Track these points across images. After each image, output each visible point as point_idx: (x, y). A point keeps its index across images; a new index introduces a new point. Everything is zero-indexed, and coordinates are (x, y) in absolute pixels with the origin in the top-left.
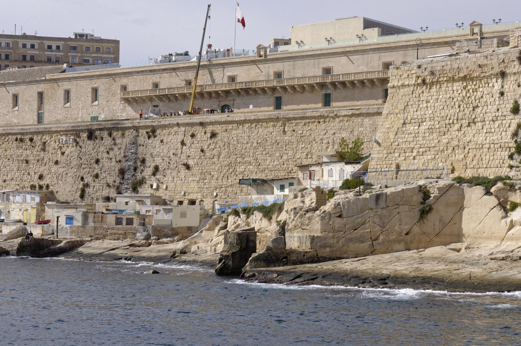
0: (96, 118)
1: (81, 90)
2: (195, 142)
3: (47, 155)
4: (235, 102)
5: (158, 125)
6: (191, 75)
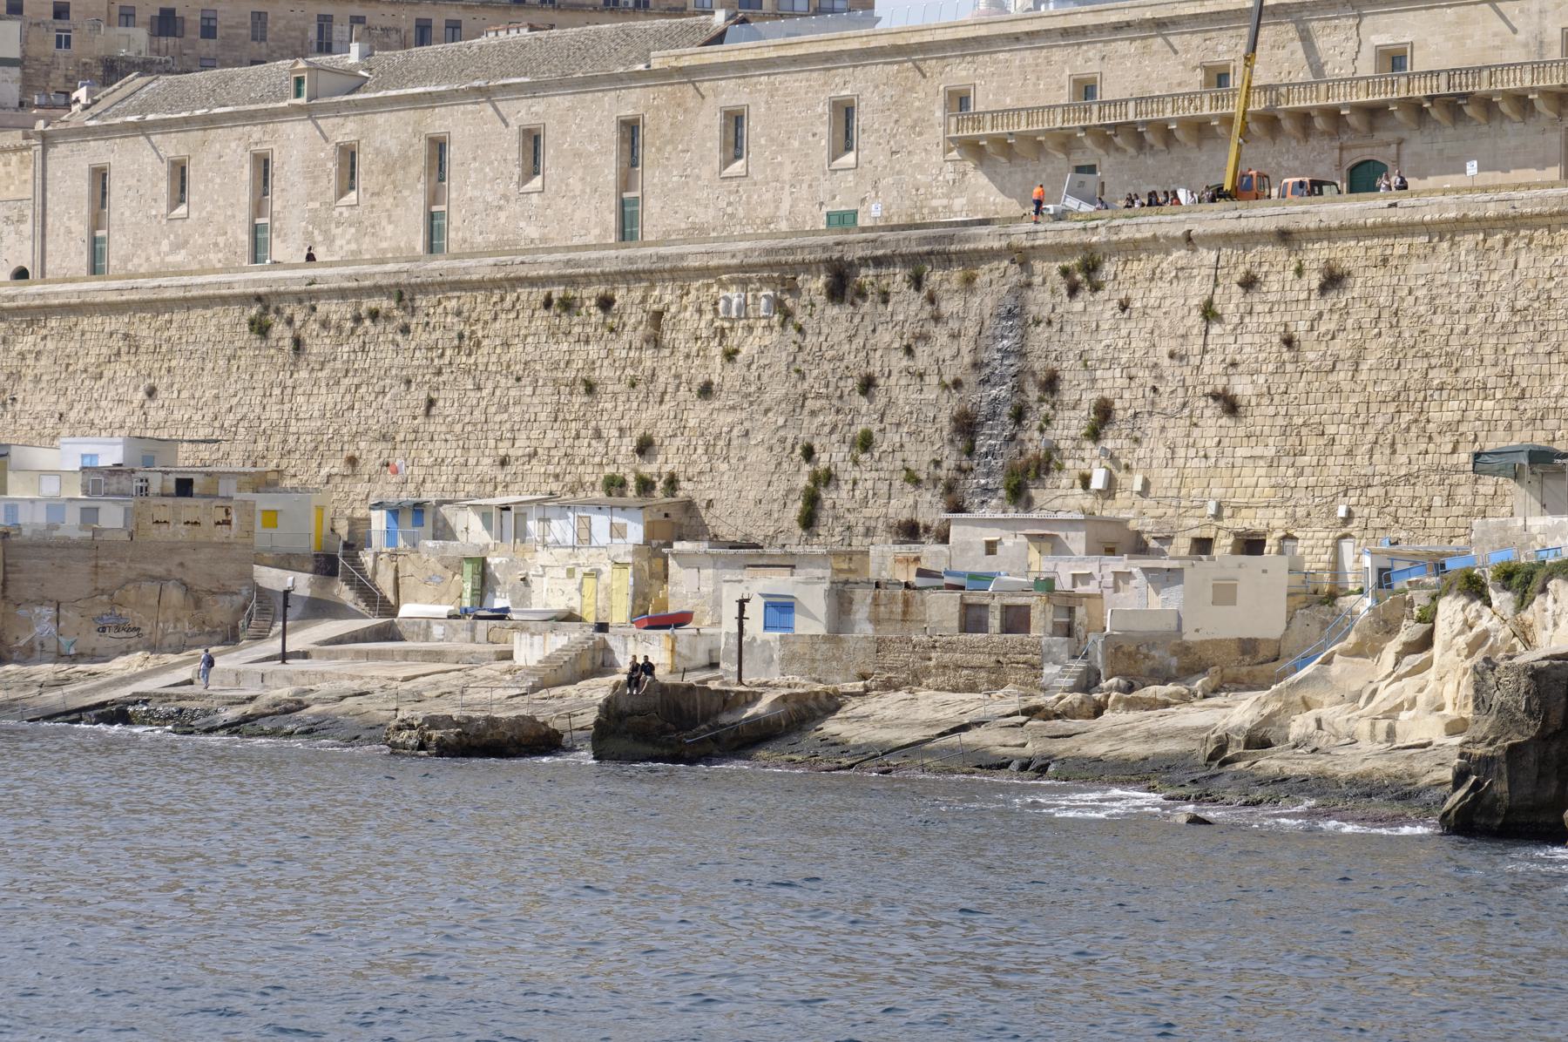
0: (849, 219)
1: (790, 111)
2: (1258, 308)
3: (668, 363)
4: (1407, 150)
5: (1108, 242)
6: (1227, 47)
